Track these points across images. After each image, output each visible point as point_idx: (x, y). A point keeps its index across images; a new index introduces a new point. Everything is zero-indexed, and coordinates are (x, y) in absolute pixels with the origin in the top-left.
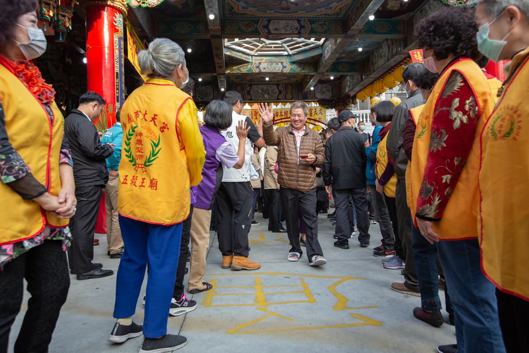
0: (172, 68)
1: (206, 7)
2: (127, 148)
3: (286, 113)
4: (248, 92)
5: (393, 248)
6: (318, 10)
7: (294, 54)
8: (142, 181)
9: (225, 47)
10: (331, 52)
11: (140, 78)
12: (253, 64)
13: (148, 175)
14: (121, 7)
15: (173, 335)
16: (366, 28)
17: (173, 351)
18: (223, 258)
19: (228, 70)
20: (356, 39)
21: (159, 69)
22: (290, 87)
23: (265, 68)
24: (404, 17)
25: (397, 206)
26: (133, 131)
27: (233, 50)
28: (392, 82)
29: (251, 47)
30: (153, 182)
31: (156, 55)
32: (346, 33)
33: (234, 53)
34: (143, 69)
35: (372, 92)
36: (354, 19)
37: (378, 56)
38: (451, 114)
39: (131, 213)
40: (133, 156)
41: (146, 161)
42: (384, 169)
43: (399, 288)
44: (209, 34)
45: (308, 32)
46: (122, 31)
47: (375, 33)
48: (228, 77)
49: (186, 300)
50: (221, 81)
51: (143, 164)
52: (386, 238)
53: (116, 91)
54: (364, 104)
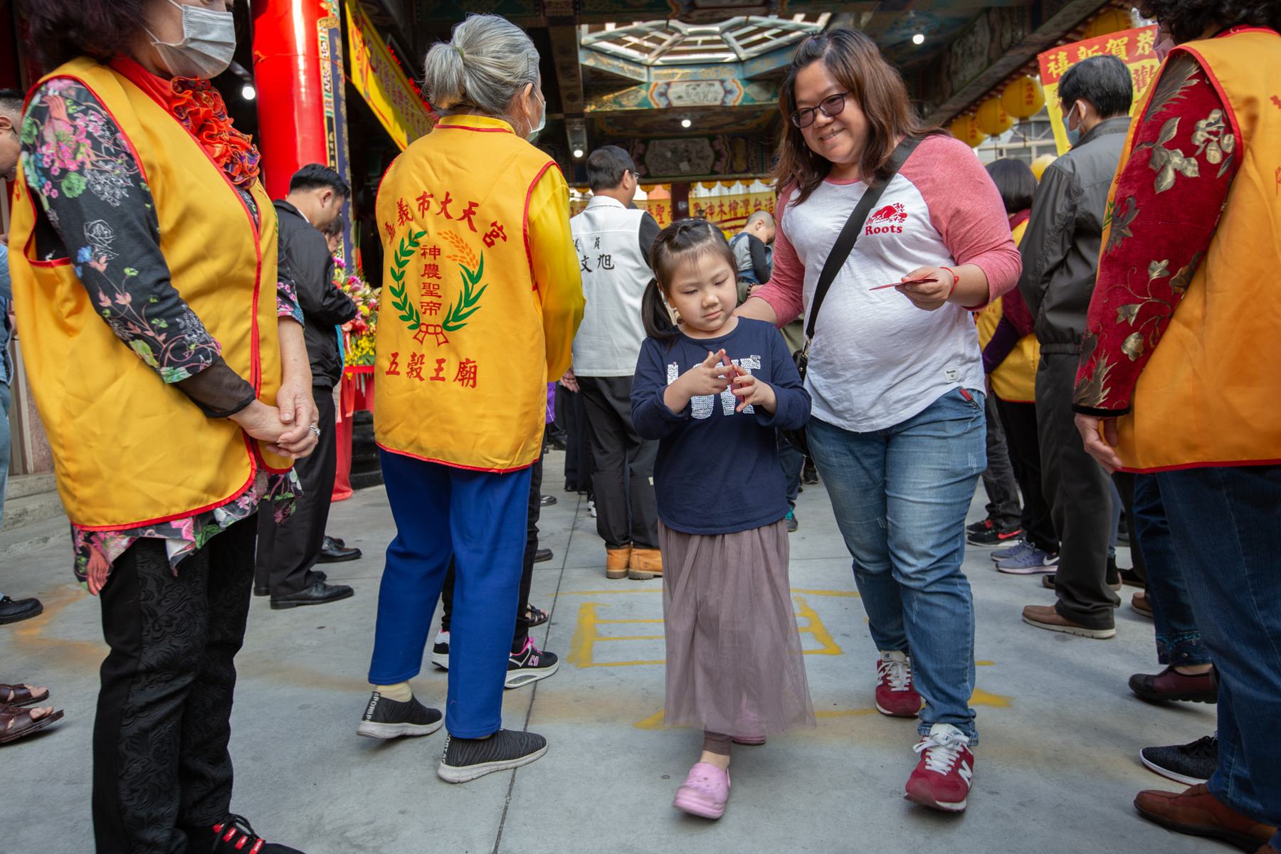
0: (508, 92)
2: (395, 284)
3: (733, 207)
5: (1016, 523)
7: (751, 59)
8: (436, 366)
9: (582, 47)
12: (652, 86)
15: (514, 732)
17: (516, 768)
18: (609, 553)
19: (591, 105)
20: (907, 13)
21: (477, 93)
23: (680, 97)
25: (1039, 420)
27: (602, 52)
29: (646, 44)
30: (468, 369)
31: (472, 56)
33: (606, 60)
39: (411, 443)
41: (448, 316)
42: (993, 332)
43: (1043, 617)
44: (544, 15)
46: (335, 13)
48: (591, 121)
49: (534, 652)
50: (574, 133)
51: (441, 324)
52: (1000, 501)
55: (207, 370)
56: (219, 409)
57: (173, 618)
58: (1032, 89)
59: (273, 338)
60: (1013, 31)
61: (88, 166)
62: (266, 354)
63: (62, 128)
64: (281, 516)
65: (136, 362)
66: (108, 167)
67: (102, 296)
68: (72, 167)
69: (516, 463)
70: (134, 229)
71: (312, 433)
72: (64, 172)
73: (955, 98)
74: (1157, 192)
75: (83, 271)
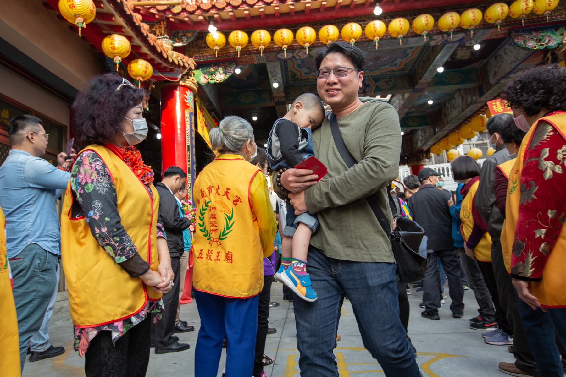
0: (241, 143)
1: (270, 76)
2: (201, 222)
5: (493, 319)
6: (382, 68)
8: (217, 255)
10: (399, 107)
11: (211, 154)
13: (223, 248)
14: (191, 86)
20: (425, 92)
21: (229, 145)
24: (476, 65)
25: (494, 272)
26: (207, 206)
28: (470, 132)
32: (414, 88)
34: (215, 145)
35: (448, 145)
36: (421, 73)
37: (450, 107)
38: (540, 164)
39: (207, 287)
40: (207, 231)
43: (509, 369)
44: (274, 101)
45: (373, 90)
47: (445, 84)
52: (484, 308)
53: (188, 163)
54: (440, 158)
55: (133, 257)
56: (136, 273)
57: (114, 366)
58: (483, 120)
59: (155, 245)
60: (471, 97)
61: (95, 180)
62: (153, 251)
63: (87, 167)
64: (156, 320)
65: (105, 256)
66: (102, 180)
67: (96, 229)
68: (90, 181)
69: (251, 294)
70: (110, 203)
71: (170, 285)
72: (86, 183)
73: (449, 125)
75: (90, 220)
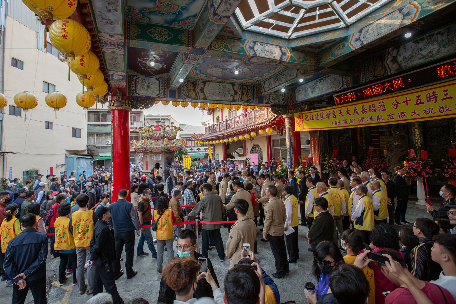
4: (202, 90)
16: (137, 33)
22: (246, 88)
74: (396, 197)
